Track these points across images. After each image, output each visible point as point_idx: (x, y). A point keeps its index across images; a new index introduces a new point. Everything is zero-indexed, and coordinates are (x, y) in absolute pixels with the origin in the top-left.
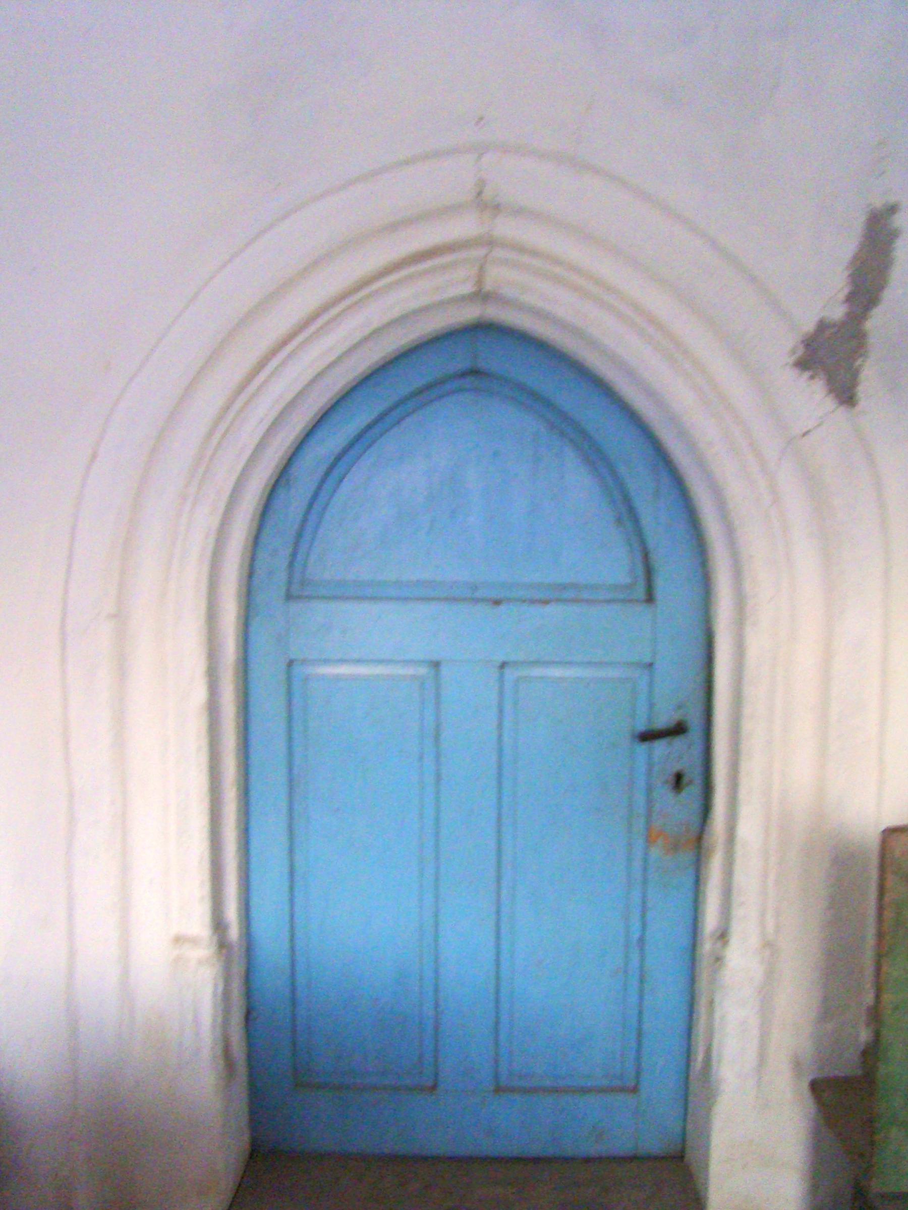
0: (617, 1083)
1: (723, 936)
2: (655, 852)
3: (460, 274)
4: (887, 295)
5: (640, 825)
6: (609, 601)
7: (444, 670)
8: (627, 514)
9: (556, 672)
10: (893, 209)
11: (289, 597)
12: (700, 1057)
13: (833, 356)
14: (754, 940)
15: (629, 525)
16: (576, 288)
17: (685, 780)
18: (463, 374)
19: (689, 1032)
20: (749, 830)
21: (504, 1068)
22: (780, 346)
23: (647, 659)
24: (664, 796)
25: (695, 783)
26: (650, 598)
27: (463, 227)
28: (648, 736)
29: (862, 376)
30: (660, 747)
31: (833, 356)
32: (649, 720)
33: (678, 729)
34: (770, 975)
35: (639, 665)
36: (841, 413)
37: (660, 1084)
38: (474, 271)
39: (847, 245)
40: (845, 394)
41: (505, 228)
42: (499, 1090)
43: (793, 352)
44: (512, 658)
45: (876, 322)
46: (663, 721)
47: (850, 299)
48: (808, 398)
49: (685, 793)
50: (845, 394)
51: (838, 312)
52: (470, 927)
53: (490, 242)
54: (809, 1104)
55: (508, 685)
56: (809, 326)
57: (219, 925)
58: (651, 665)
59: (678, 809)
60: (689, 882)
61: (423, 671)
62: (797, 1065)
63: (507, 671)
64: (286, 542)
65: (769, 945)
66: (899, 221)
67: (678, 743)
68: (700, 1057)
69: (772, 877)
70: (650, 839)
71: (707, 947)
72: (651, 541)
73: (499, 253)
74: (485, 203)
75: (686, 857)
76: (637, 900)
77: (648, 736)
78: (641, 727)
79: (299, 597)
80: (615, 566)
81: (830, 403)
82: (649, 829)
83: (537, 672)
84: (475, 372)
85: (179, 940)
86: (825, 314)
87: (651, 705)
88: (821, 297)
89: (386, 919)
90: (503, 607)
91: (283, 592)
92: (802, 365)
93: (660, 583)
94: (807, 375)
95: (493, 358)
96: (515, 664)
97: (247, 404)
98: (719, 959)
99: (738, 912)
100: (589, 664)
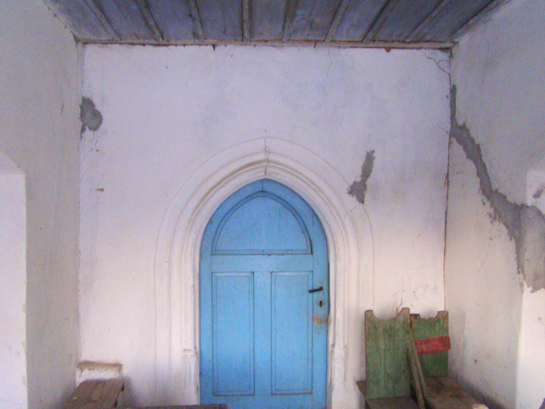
0: (306, 391)
1: (333, 346)
2: (315, 323)
3: (260, 170)
4: (371, 174)
5: (310, 316)
6: (301, 254)
7: (256, 275)
8: (305, 230)
9: (286, 274)
10: (373, 152)
11: (212, 254)
12: (329, 381)
13: (358, 190)
14: (342, 346)
15: (306, 233)
16: (290, 173)
17: (323, 303)
18: (260, 192)
19: (326, 376)
20: (339, 316)
21: (274, 388)
22: (345, 187)
23: (311, 269)
24: (317, 307)
25: (325, 304)
26: (312, 253)
27: (262, 157)
28: (312, 291)
29: (365, 196)
30: (316, 294)
31: (358, 190)
32: (312, 286)
33: (321, 289)
34: (346, 355)
35: (310, 271)
36: (361, 204)
37: (318, 387)
38: (264, 170)
39: (361, 162)
40: (362, 201)
41: (272, 157)
42: (272, 394)
43: (348, 189)
44: (274, 270)
45: (370, 182)
46: (316, 287)
47: (362, 176)
48: (352, 201)
49: (323, 307)
50: (362, 201)
51: (359, 179)
52: (269, 344)
53: (268, 161)
54: (357, 387)
55: (273, 278)
56: (351, 183)
57: (195, 348)
58: (312, 272)
59: (320, 311)
60: (325, 332)
61: (249, 274)
62: (354, 379)
63: (273, 274)
64: (214, 241)
65: (346, 347)
66: (374, 155)
67: (321, 293)
68: (329, 381)
69: (346, 328)
70: (313, 320)
71: (330, 349)
72: (312, 238)
73: (270, 164)
74: (266, 150)
75: (324, 325)
76: (310, 337)
77: (312, 291)
78: (311, 289)
79: (214, 255)
80: (302, 244)
81: (358, 203)
82: (313, 318)
83: (281, 274)
84: (263, 191)
85: (185, 350)
86: (356, 180)
87: (313, 283)
88: (356, 176)
89: (237, 346)
90: (272, 256)
91: (210, 253)
92: (350, 193)
93: (314, 249)
94: (351, 195)
95: (269, 188)
96: (275, 272)
97: (204, 205)
98: (333, 352)
99: (337, 338)
100: (296, 271)
